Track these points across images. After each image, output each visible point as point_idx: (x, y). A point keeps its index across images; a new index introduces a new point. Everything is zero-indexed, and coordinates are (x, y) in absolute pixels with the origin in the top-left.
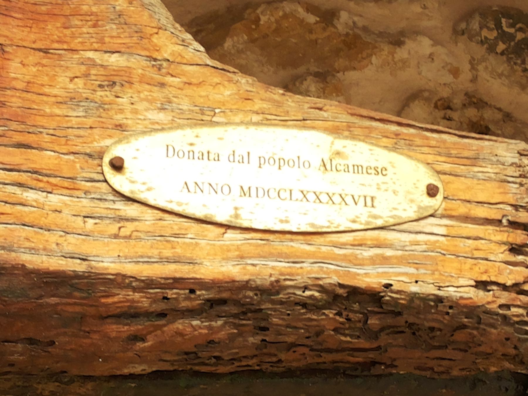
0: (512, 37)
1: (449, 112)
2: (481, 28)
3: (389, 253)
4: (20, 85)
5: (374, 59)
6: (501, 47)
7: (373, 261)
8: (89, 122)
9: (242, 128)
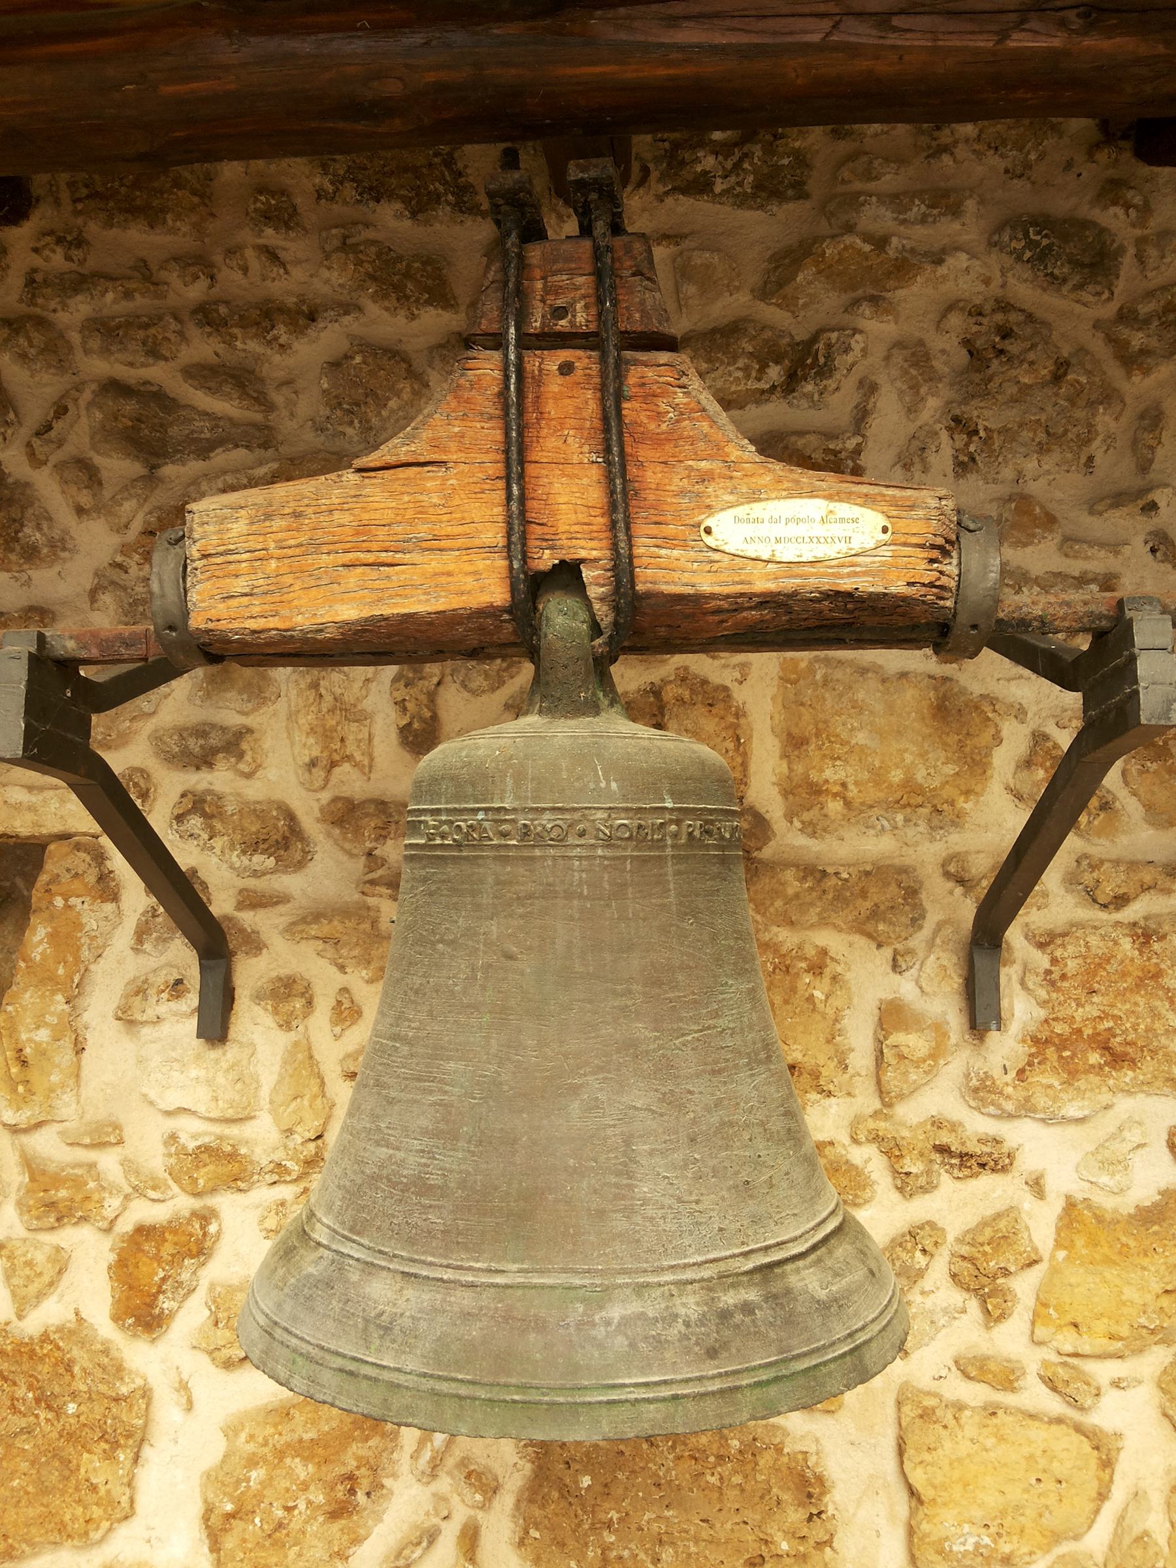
0: (1038, 244)
1: (980, 318)
2: (1011, 240)
3: (858, 569)
4: (653, 486)
5: (918, 278)
7: (849, 575)
8: (692, 505)
9: (776, 502)
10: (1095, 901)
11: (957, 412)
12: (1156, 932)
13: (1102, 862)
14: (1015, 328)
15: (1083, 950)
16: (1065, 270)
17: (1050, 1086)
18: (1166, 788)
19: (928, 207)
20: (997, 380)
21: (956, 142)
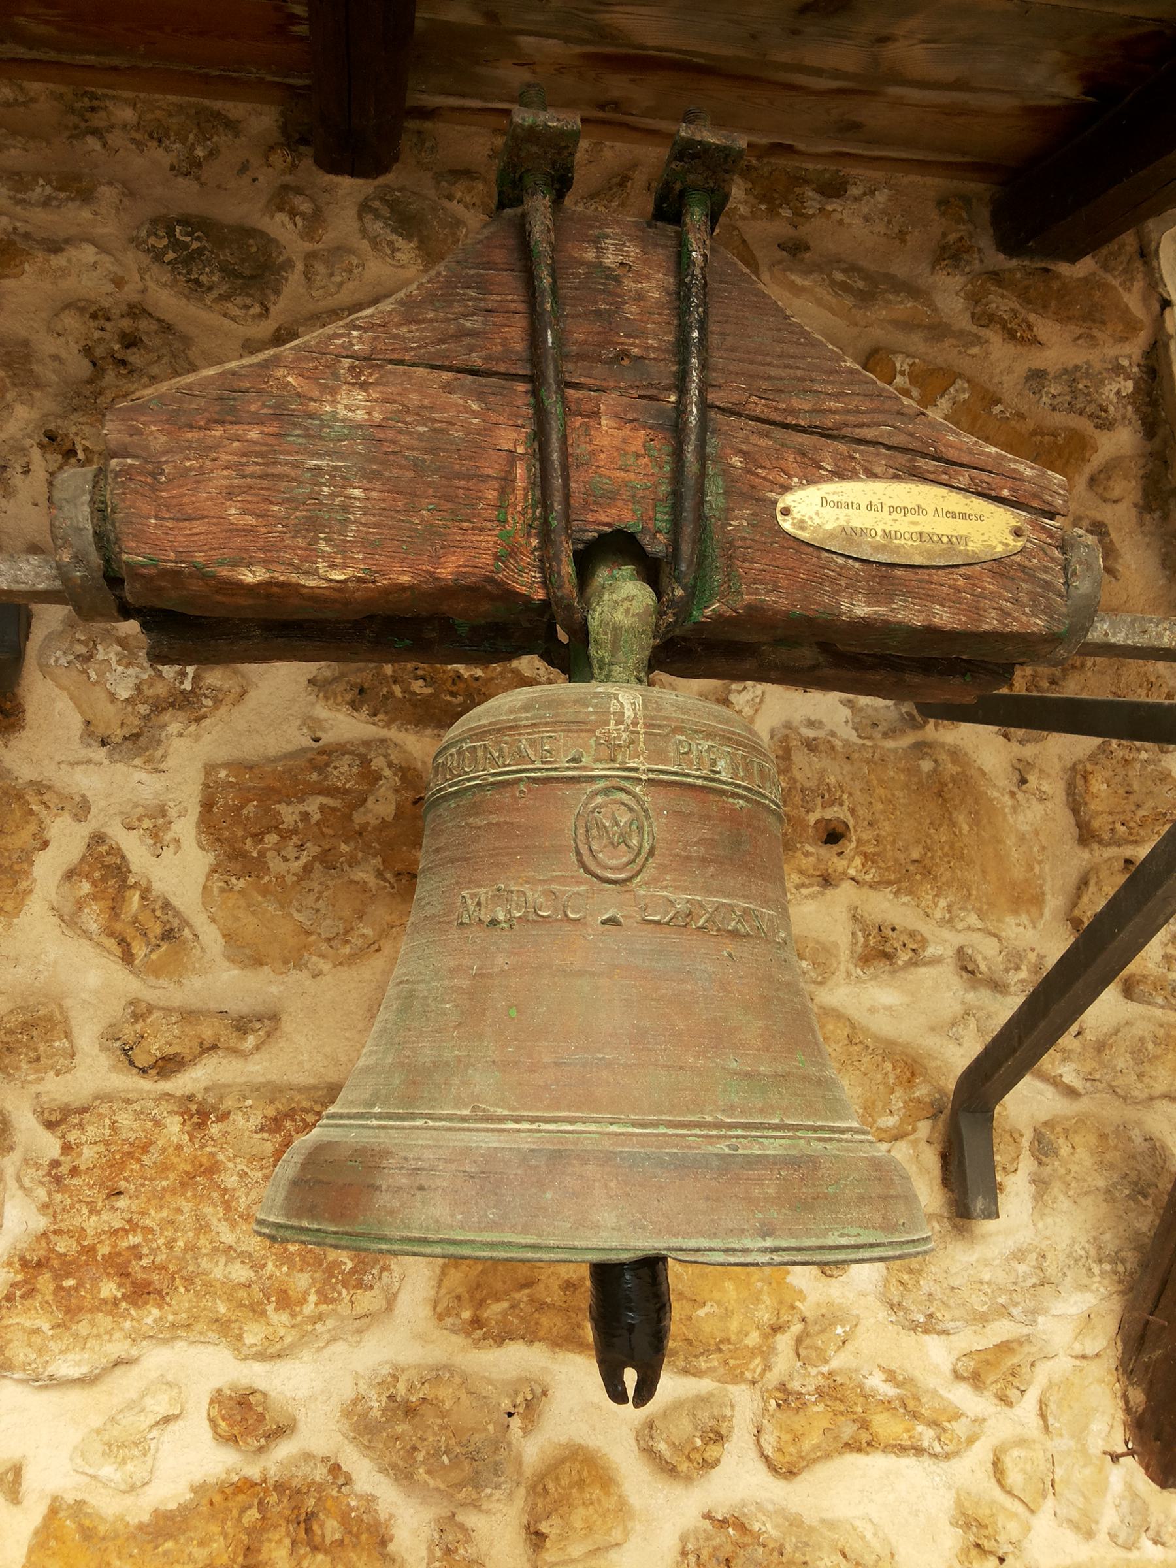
0: (186, 246)
2: (148, 236)
6: (171, 255)
10: (131, 1063)
11: (52, 426)
12: (215, 1109)
13: (150, 1009)
14: (145, 339)
15: (107, 1132)
16: (215, 279)
17: (37, 1331)
18: (253, 913)
19: (55, 188)
20: (110, 394)
21: (112, 127)
